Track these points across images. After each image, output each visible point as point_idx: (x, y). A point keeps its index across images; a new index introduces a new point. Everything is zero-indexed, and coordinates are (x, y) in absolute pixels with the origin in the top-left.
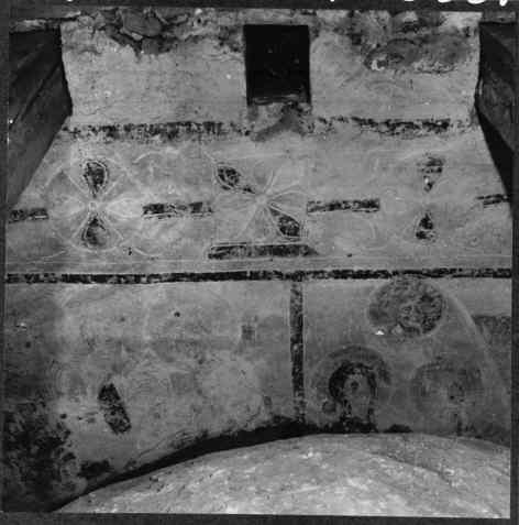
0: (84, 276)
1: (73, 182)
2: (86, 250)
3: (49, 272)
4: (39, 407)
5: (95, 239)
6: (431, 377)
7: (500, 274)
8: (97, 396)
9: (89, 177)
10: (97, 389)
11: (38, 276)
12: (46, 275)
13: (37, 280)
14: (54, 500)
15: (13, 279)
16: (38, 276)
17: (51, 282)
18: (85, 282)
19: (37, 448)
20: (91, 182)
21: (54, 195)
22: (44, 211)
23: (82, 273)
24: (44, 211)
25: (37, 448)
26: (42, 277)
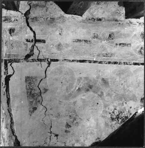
0: (139, 63)
1: (16, 53)
2: (139, 55)
3: (130, 62)
4: (124, 104)
5: (142, 53)
6: (57, 71)
7: (142, 64)
8: (140, 101)
9: (142, 36)
10: (140, 99)
11: (127, 63)
12: (129, 62)
13: (127, 64)
14: (43, 94)
15: (142, 64)
16: (127, 63)
17: (130, 65)
18: (139, 65)
19: (121, 120)
20: (142, 37)
21: (133, 40)
22: (130, 44)
23: (138, 62)
24: (130, 44)
25: (121, 120)
26: (128, 63)
